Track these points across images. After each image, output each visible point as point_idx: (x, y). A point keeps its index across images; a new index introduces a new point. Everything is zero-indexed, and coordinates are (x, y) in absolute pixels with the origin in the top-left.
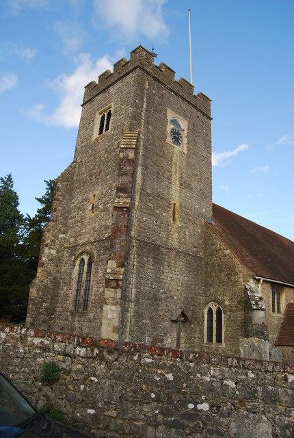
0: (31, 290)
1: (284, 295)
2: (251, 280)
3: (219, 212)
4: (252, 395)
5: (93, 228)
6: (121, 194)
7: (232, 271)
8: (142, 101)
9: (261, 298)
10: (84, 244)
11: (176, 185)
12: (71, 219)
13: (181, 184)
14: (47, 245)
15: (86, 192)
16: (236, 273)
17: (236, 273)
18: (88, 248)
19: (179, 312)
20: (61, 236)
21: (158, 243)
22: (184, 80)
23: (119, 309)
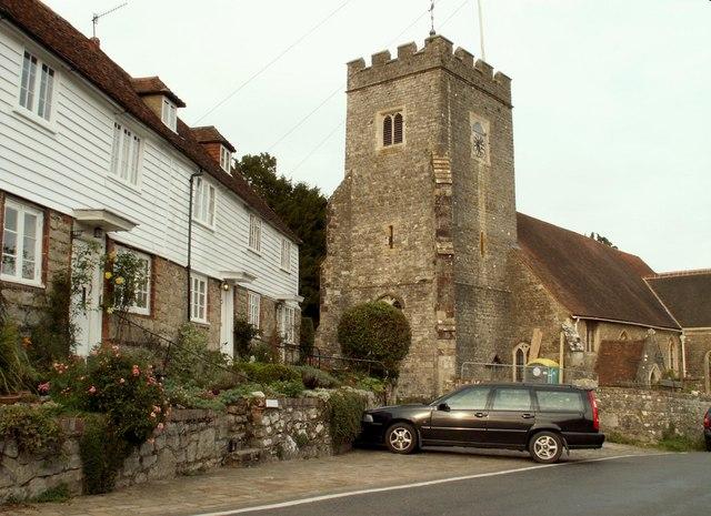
0: (316, 339)
1: (598, 332)
2: (568, 320)
3: (529, 229)
4: (609, 404)
5: (396, 268)
6: (441, 238)
7: (546, 310)
8: (446, 113)
9: (578, 339)
10: (385, 286)
11: (482, 211)
12: (355, 251)
13: (487, 208)
14: (328, 285)
15: (376, 220)
16: (550, 312)
17: (550, 312)
18: (391, 291)
19: (493, 355)
20: (344, 273)
21: (470, 283)
22: (483, 63)
23: (454, 358)
